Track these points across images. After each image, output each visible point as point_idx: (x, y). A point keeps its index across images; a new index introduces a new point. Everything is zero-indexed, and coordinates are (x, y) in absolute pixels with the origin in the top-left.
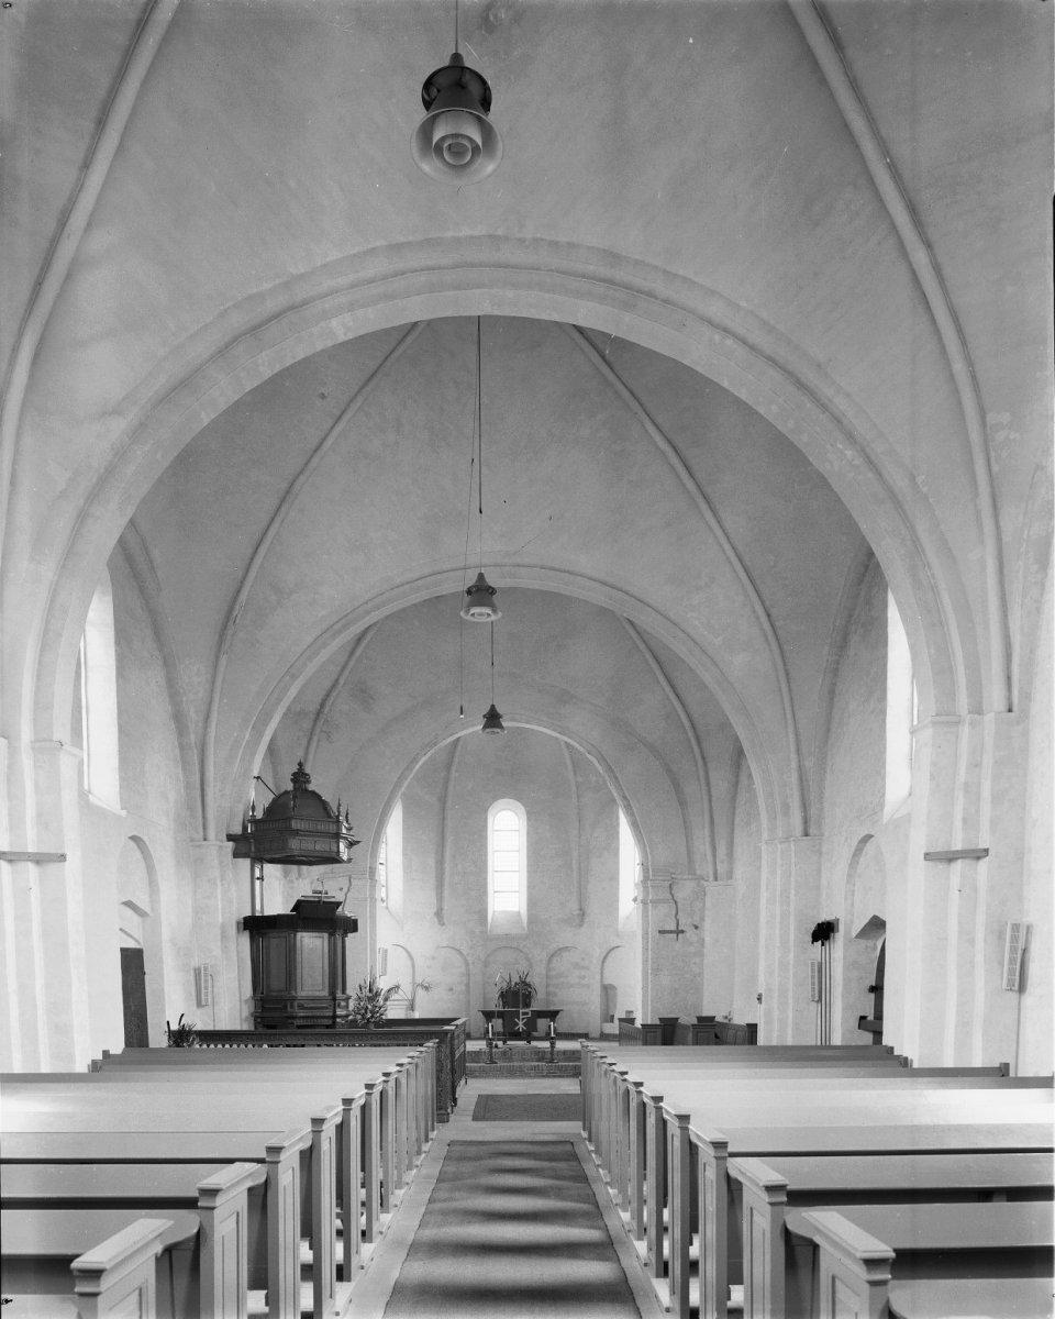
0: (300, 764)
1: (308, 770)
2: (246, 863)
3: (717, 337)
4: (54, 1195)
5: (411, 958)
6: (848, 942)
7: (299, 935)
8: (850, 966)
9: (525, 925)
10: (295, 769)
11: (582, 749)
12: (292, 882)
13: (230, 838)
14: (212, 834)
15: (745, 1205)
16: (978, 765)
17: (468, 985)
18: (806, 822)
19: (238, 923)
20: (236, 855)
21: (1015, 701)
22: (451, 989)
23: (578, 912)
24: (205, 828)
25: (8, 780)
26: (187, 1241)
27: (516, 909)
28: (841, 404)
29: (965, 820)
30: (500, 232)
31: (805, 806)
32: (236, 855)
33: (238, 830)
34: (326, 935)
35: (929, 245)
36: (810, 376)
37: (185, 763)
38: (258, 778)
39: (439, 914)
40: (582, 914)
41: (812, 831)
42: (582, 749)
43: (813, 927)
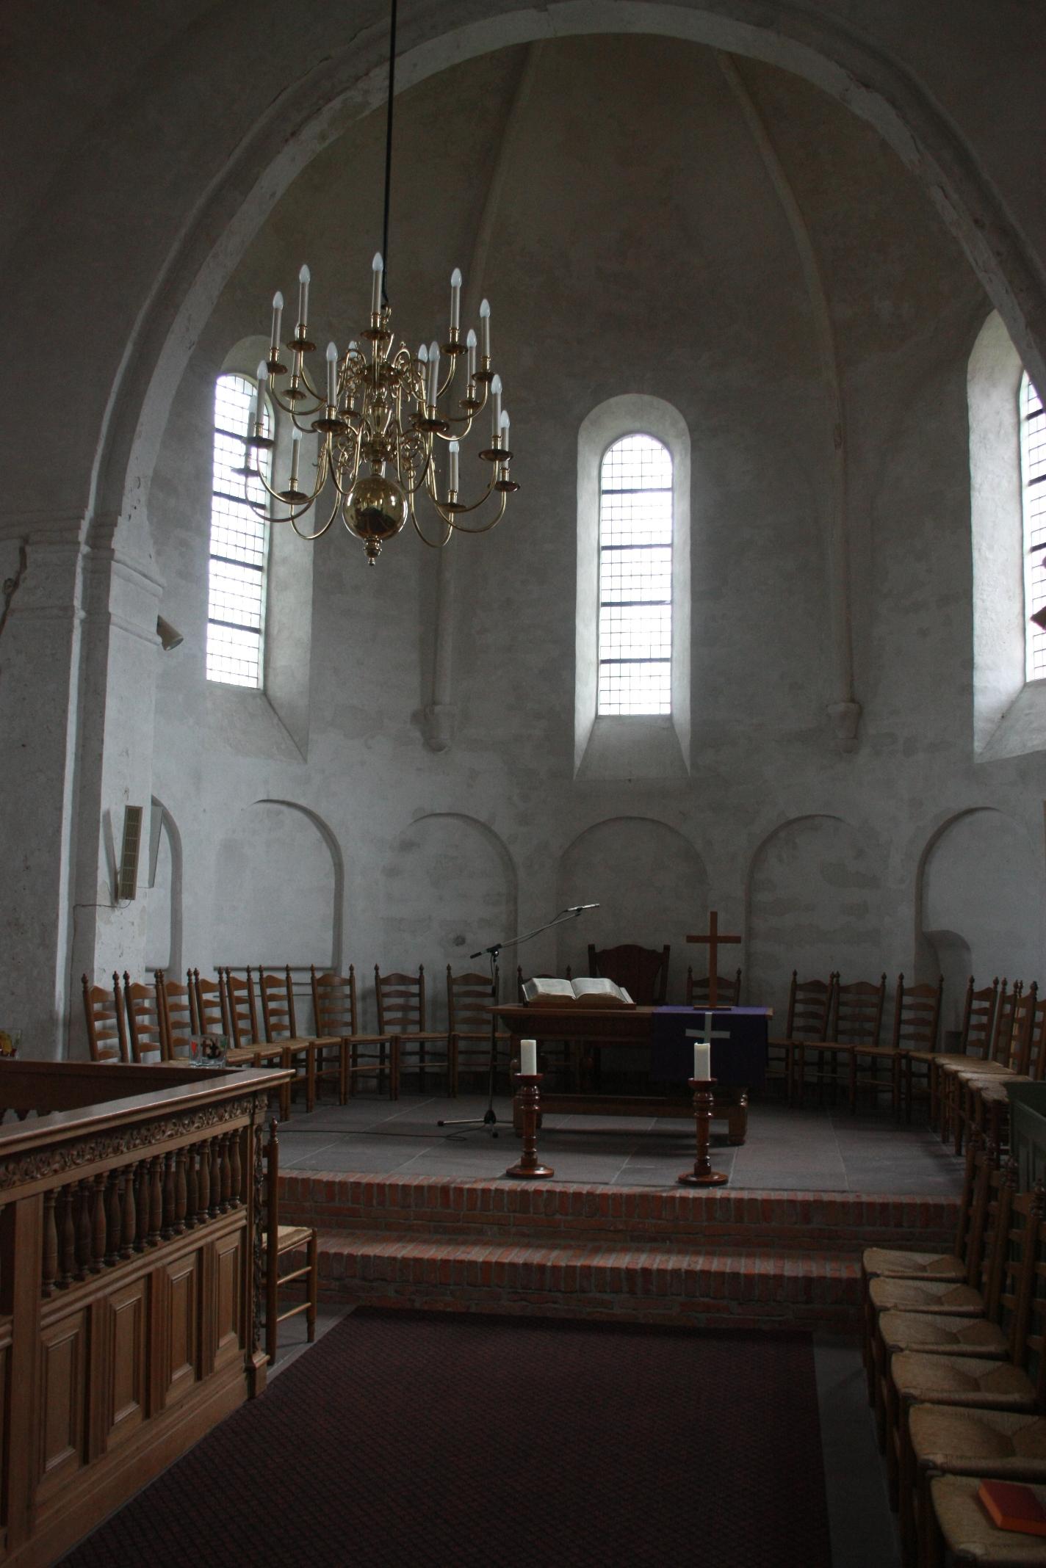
22: (460, 941)
23: (841, 707)
39: (425, 718)
40: (857, 711)
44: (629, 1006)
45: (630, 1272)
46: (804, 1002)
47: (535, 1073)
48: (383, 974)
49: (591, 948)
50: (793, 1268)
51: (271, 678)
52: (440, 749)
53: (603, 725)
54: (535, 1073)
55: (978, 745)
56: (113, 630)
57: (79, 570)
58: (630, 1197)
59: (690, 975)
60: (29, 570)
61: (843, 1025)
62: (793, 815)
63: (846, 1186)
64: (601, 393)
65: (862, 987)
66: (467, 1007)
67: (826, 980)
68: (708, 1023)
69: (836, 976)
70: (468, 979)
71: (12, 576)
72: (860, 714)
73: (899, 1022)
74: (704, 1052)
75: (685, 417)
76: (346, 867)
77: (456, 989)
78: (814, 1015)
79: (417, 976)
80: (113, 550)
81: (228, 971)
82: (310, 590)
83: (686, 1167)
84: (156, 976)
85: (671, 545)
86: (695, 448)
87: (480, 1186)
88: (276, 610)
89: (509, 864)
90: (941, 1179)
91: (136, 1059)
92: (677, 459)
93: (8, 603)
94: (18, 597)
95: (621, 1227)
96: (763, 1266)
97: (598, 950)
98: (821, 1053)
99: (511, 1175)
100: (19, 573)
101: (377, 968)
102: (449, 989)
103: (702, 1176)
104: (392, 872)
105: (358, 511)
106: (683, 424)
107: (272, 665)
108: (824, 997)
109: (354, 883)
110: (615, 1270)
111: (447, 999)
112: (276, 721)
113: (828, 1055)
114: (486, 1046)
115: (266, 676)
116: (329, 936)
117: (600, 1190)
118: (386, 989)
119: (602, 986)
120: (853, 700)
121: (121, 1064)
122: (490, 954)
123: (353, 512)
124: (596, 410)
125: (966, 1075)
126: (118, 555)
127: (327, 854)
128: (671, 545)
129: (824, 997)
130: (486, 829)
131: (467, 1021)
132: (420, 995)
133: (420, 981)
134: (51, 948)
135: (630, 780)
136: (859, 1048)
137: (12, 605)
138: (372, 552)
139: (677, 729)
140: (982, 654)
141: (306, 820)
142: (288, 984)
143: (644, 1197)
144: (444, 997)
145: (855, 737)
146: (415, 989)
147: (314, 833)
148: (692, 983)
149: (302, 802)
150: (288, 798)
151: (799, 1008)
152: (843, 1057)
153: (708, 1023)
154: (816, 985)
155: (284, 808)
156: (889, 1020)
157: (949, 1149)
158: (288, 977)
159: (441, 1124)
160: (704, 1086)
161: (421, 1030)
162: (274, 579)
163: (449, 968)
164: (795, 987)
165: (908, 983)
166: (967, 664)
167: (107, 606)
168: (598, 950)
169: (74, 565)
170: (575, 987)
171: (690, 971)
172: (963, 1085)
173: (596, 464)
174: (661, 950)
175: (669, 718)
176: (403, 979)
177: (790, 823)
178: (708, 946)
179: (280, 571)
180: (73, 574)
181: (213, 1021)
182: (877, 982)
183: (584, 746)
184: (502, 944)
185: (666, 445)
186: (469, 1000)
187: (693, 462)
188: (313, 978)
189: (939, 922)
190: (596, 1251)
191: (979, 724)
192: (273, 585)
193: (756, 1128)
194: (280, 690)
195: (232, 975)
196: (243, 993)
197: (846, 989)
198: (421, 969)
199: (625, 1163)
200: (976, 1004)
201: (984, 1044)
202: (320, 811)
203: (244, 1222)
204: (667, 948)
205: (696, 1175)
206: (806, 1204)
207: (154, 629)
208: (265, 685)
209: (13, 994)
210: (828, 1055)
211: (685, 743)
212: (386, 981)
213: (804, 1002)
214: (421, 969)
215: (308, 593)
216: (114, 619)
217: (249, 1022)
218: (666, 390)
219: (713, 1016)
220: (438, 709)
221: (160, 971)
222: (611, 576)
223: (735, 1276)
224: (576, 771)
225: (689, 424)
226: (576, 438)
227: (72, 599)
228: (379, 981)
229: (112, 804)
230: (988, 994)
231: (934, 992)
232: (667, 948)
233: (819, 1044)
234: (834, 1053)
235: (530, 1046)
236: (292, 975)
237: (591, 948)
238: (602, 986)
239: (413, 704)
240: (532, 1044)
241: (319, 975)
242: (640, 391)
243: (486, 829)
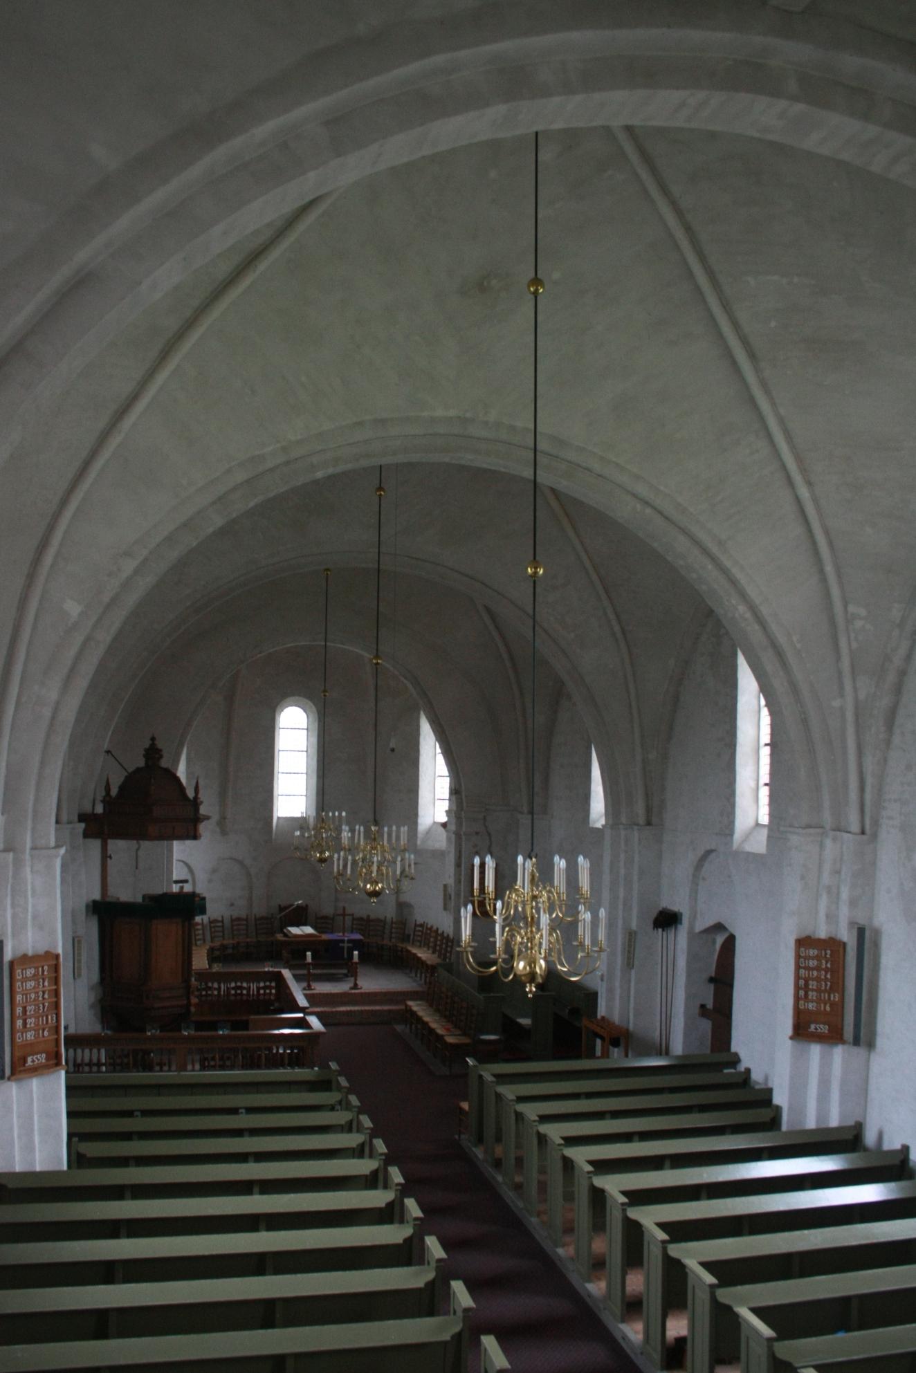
0: (153, 739)
1: (159, 745)
3: (638, 506)
4: (660, 1106)
5: (183, 862)
6: (692, 936)
8: (692, 958)
10: (147, 744)
11: (396, 672)
15: (743, 1336)
16: (838, 872)
17: (250, 899)
18: (649, 810)
19: (87, 906)
20: (86, 835)
21: (867, 827)
22: (232, 905)
28: (736, 571)
29: (827, 916)
30: (468, 415)
31: (648, 796)
32: (86, 835)
33: (87, 808)
35: (809, 484)
36: (715, 550)
38: (108, 752)
41: (654, 820)
42: (396, 672)
43: (654, 914)
49: (280, 906)
50: (386, 1008)
55: (419, 842)
65: (378, 920)
67: (365, 917)
68: (346, 942)
69: (368, 916)
73: (391, 933)
90: (414, 984)
92: (310, 719)
96: (378, 1008)
99: (351, 988)
104: (210, 881)
125: (419, 955)
130: (241, 863)
132: (223, 926)
133: (222, 921)
140: (421, 811)
141: (184, 866)
151: (354, 926)
153: (346, 942)
154: (361, 919)
156: (387, 931)
157: (413, 975)
161: (224, 939)
165: (394, 920)
166: (416, 815)
170: (302, 931)
172: (419, 959)
182: (383, 918)
185: (305, 711)
189: (405, 898)
191: (420, 835)
197: (373, 921)
200: (418, 928)
201: (420, 942)
202: (189, 861)
204: (307, 906)
218: (310, 697)
223: (372, 1011)
230: (421, 925)
231: (402, 923)
237: (280, 906)
238: (308, 930)
242: (300, 696)
243: (241, 863)
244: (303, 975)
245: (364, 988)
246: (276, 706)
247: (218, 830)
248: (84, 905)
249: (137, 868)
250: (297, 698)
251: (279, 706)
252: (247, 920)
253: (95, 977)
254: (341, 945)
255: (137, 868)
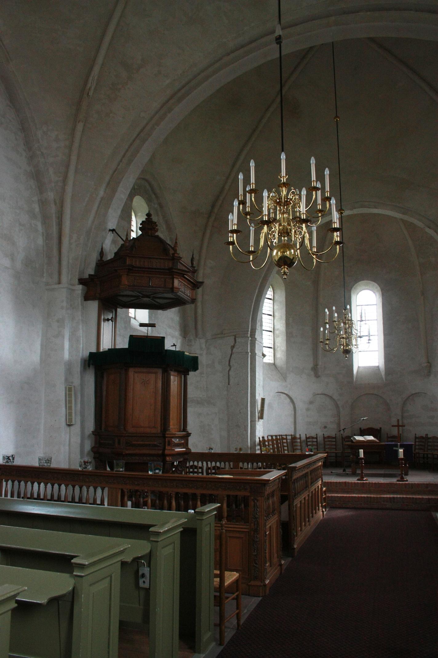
2: (94, 306)
4: (102, 518)
7: (131, 373)
9: (384, 377)
12: (190, 341)
13: (82, 281)
14: (64, 278)
20: (87, 297)
22: (325, 427)
23: (426, 364)
24: (60, 274)
25: (73, 285)
26: (69, 593)
27: (377, 365)
32: (87, 297)
34: (160, 371)
37: (45, 219)
38: (113, 230)
39: (315, 369)
40: (430, 366)
44: (378, 442)
45: (390, 498)
46: (418, 442)
47: (363, 457)
48: (307, 436)
49: (360, 428)
51: (276, 360)
52: (319, 377)
53: (361, 369)
54: (363, 457)
56: (257, 357)
57: (249, 343)
58: (387, 483)
59: (387, 435)
60: (237, 344)
61: (429, 448)
62: (414, 392)
63: (435, 481)
64: (357, 281)
66: (328, 445)
67: (424, 436)
68: (399, 446)
69: (427, 435)
70: (329, 437)
71: (233, 345)
72: (430, 366)
74: (401, 452)
75: (380, 286)
76: (297, 409)
77: (326, 440)
78: (421, 445)
79: (316, 437)
80: (256, 338)
81: (281, 435)
82: (285, 337)
83: (399, 478)
84: (271, 437)
85: (377, 320)
86: (383, 295)
87: (353, 482)
88: (276, 342)
89: (337, 406)
91: (284, 452)
93: (232, 351)
94: (234, 350)
95: (385, 490)
97: (362, 429)
98: (424, 455)
100: (234, 345)
101: (306, 435)
102: (324, 440)
103: (402, 479)
104: (308, 410)
105: (344, 349)
106: (379, 288)
107: (276, 356)
108: (424, 440)
109: (299, 413)
110: (387, 497)
111: (323, 442)
112: (278, 371)
113: (425, 456)
114: (334, 455)
115: (274, 360)
116: (293, 426)
117: (380, 482)
118: (308, 440)
119: (371, 438)
120: (428, 362)
121: (288, 453)
122: (343, 431)
123: (343, 349)
124: (356, 285)
126: (257, 339)
127: (292, 406)
128: (377, 320)
129: (424, 440)
130: (331, 397)
131: (328, 448)
132: (317, 442)
133: (316, 438)
134: (247, 431)
135: (369, 384)
136: (434, 453)
137: (233, 351)
138: (346, 357)
139: (381, 370)
142: (286, 439)
143: (390, 483)
144: (323, 442)
145: (430, 372)
146: (315, 440)
147: (288, 400)
148: (388, 437)
149: (286, 392)
150: (283, 391)
151: (417, 443)
152: (429, 456)
153: (399, 446)
154: (422, 437)
155: (281, 394)
158: (286, 438)
159: (332, 472)
160: (402, 459)
162: (275, 334)
163: (324, 434)
164: (416, 438)
167: (255, 351)
168: (362, 429)
169: (248, 342)
170: (365, 438)
171: (387, 434)
173: (355, 298)
174: (379, 429)
175: (378, 367)
176: (313, 438)
177: (412, 394)
178: (397, 428)
179: (277, 332)
180: (248, 344)
181: (285, 446)
183: (356, 375)
184: (346, 428)
186: (328, 443)
187: (382, 299)
188: (292, 438)
190: (381, 495)
192: (275, 336)
193: (410, 472)
194: (279, 363)
195: (283, 436)
196: (285, 441)
197: (430, 438)
198: (317, 435)
199: (382, 478)
202: (291, 394)
203: (321, 483)
204: (381, 428)
205: (401, 479)
206: (427, 484)
207: (261, 355)
208: (274, 362)
209: (238, 442)
210: (425, 456)
211: (383, 373)
212: (309, 438)
213: (418, 442)
214: (317, 435)
215: (285, 338)
216: (257, 354)
217: (300, 447)
219: (400, 444)
220: (318, 367)
221: (272, 436)
222: (360, 326)
224: (354, 381)
225: (381, 288)
226: (351, 293)
227: (248, 350)
228: (307, 438)
229: (258, 398)
232: (381, 428)
233: (423, 452)
234: (427, 454)
235: (361, 451)
236: (288, 437)
237: (360, 428)
238: (371, 438)
239: (311, 365)
240: (362, 451)
241: (293, 436)
243: (331, 397)
244: (184, 376)
245: (408, 481)
246: (352, 288)
247: (312, 373)
248: (80, 359)
249: (229, 384)
250: (365, 281)
251: (353, 288)
252: (335, 438)
253: (90, 426)
254: (394, 448)
255: (229, 384)
